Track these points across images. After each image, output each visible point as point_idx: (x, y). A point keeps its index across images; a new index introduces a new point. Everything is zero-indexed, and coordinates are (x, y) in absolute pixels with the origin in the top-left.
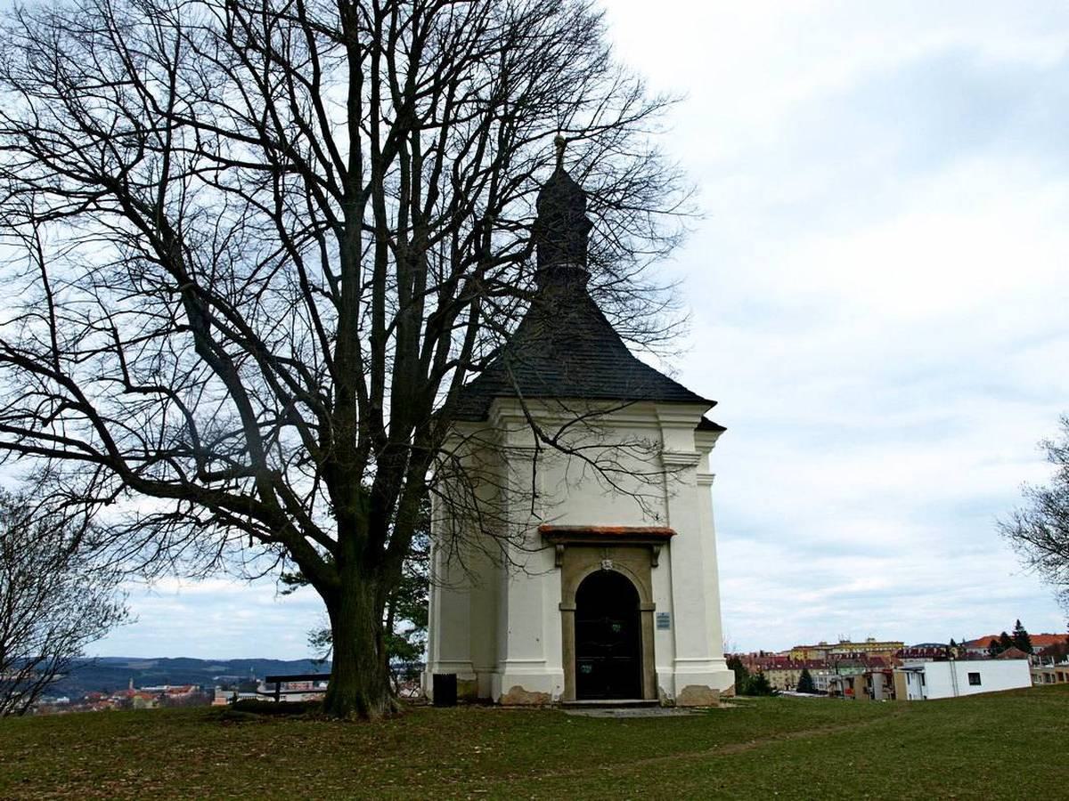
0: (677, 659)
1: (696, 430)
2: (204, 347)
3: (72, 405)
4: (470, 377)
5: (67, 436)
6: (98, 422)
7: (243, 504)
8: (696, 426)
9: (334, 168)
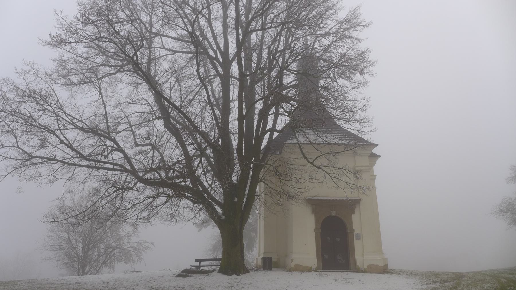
0: (364, 253)
1: (369, 156)
2: (168, 126)
3: (116, 150)
4: (276, 134)
5: (284, 76)
6: (126, 157)
7: (186, 188)
8: (369, 155)
9: (218, 52)
